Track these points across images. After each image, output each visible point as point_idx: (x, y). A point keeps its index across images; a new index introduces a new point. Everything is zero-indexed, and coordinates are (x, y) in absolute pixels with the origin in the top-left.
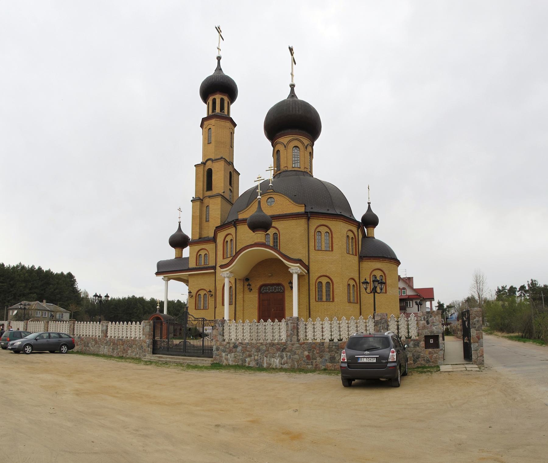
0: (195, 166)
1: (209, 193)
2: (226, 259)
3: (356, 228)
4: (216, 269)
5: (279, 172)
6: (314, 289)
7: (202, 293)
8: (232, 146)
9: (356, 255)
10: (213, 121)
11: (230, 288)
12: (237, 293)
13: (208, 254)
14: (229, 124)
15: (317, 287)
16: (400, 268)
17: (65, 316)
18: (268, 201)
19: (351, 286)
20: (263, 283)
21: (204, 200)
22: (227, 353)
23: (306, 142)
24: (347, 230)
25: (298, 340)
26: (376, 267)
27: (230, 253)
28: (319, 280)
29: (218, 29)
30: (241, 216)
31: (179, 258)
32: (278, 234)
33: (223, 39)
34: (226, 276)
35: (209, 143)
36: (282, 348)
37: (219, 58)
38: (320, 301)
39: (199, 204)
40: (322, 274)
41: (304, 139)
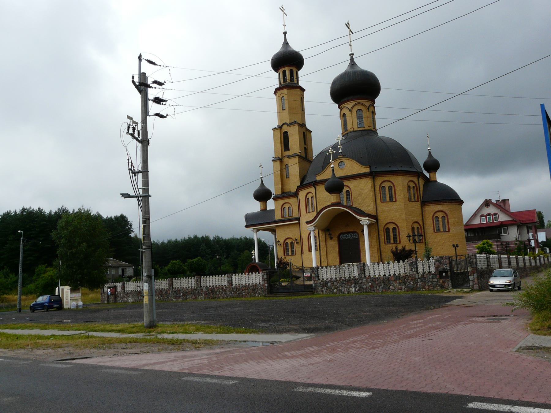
0: (272, 129)
1: (287, 153)
2: (309, 213)
5: (346, 132)
7: (289, 241)
8: (303, 110)
9: (418, 201)
10: (285, 91)
11: (315, 237)
12: (321, 241)
13: (291, 206)
14: (298, 92)
15: (385, 232)
16: (464, 207)
17: (128, 270)
18: (340, 164)
19: (416, 228)
23: (367, 103)
24: (407, 181)
25: (365, 276)
26: (438, 210)
28: (387, 227)
29: (282, 9)
30: (319, 178)
31: (264, 210)
32: (350, 191)
34: (311, 230)
37: (285, 33)
38: (389, 243)
39: (279, 163)
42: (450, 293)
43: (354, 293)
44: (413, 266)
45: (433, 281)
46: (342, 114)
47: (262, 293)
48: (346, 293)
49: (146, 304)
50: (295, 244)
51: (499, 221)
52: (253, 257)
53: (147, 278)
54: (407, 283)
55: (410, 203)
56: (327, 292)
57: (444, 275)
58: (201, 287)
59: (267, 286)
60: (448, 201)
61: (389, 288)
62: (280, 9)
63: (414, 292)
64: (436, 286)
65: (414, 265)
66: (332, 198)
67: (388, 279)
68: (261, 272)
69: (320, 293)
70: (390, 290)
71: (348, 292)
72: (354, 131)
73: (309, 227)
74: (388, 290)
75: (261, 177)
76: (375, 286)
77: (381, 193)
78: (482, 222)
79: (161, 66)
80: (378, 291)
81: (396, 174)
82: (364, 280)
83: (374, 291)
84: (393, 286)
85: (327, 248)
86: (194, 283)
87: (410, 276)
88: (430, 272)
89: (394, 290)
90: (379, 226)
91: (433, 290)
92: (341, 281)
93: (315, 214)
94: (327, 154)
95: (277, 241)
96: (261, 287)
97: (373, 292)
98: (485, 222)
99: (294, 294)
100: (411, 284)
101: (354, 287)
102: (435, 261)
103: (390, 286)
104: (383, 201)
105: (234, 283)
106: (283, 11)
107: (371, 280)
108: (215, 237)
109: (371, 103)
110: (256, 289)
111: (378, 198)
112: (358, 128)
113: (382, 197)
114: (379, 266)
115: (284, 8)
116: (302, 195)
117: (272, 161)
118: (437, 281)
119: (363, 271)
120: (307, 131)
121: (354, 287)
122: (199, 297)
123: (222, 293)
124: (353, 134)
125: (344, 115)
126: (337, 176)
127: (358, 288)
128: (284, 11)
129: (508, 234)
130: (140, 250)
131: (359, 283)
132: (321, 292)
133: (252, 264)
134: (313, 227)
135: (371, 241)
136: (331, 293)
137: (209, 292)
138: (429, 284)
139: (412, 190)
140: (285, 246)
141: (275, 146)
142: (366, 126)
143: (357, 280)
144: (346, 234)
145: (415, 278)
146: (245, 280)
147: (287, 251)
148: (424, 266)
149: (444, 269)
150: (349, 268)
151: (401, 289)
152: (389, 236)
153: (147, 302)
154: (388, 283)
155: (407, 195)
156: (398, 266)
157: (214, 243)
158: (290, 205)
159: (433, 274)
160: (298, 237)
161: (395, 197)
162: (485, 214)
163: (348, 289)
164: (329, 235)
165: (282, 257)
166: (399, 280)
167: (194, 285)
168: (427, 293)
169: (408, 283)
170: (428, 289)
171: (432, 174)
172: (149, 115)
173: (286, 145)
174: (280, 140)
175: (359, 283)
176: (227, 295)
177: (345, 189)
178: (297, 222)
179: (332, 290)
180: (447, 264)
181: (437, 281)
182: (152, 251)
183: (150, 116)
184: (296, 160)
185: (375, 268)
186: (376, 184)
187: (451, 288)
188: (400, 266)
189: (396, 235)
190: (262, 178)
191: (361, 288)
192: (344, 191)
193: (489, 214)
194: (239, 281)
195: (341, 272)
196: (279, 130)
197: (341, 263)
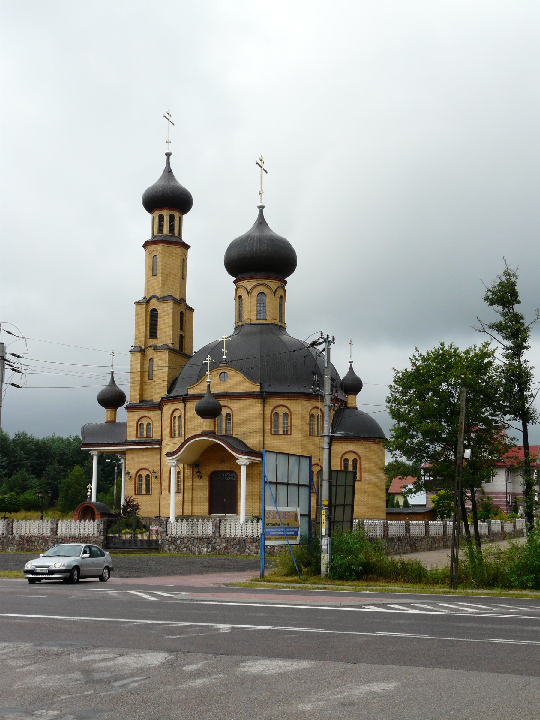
1: (152, 342)
2: (173, 439)
4: (161, 445)
5: (240, 324)
7: (144, 474)
8: (183, 278)
10: (159, 247)
12: (186, 480)
14: (179, 250)
18: (221, 376)
21: (146, 351)
23: (274, 284)
24: (310, 408)
25: (220, 535)
26: (348, 450)
29: (168, 117)
32: (231, 414)
34: (172, 464)
35: (154, 275)
36: (209, 541)
37: (168, 155)
46: (238, 295)
48: (197, 553)
52: (88, 494)
55: (312, 438)
58: (12, 534)
59: (102, 538)
61: (244, 551)
66: (205, 425)
68: (96, 520)
71: (200, 553)
73: (170, 461)
75: (112, 370)
76: (229, 547)
77: (273, 421)
80: (232, 553)
82: (218, 540)
84: (249, 549)
85: (194, 492)
86: (3, 529)
92: (193, 538)
93: (182, 440)
94: (204, 362)
95: (127, 471)
101: (207, 547)
104: (275, 432)
105: (59, 532)
107: (226, 540)
108: (19, 434)
111: (268, 427)
112: (257, 319)
113: (273, 427)
116: (168, 409)
119: (218, 529)
120: (187, 310)
121: (207, 547)
122: (8, 547)
123: (42, 544)
124: (248, 328)
125: (240, 297)
127: (211, 548)
131: (212, 542)
132: (168, 551)
134: (174, 461)
136: (180, 552)
137: (23, 542)
139: (316, 420)
140: (137, 480)
141: (136, 329)
142: (270, 317)
144: (228, 474)
146: (75, 529)
147: (139, 487)
151: (257, 553)
155: (307, 427)
157: (16, 447)
158: (149, 420)
161: (291, 429)
163: (200, 549)
165: (131, 497)
166: (256, 543)
167: (3, 531)
173: (153, 332)
175: (212, 542)
177: (224, 411)
178: (158, 446)
184: (165, 355)
186: (266, 409)
190: (113, 372)
191: (214, 548)
194: (66, 529)
195: (193, 528)
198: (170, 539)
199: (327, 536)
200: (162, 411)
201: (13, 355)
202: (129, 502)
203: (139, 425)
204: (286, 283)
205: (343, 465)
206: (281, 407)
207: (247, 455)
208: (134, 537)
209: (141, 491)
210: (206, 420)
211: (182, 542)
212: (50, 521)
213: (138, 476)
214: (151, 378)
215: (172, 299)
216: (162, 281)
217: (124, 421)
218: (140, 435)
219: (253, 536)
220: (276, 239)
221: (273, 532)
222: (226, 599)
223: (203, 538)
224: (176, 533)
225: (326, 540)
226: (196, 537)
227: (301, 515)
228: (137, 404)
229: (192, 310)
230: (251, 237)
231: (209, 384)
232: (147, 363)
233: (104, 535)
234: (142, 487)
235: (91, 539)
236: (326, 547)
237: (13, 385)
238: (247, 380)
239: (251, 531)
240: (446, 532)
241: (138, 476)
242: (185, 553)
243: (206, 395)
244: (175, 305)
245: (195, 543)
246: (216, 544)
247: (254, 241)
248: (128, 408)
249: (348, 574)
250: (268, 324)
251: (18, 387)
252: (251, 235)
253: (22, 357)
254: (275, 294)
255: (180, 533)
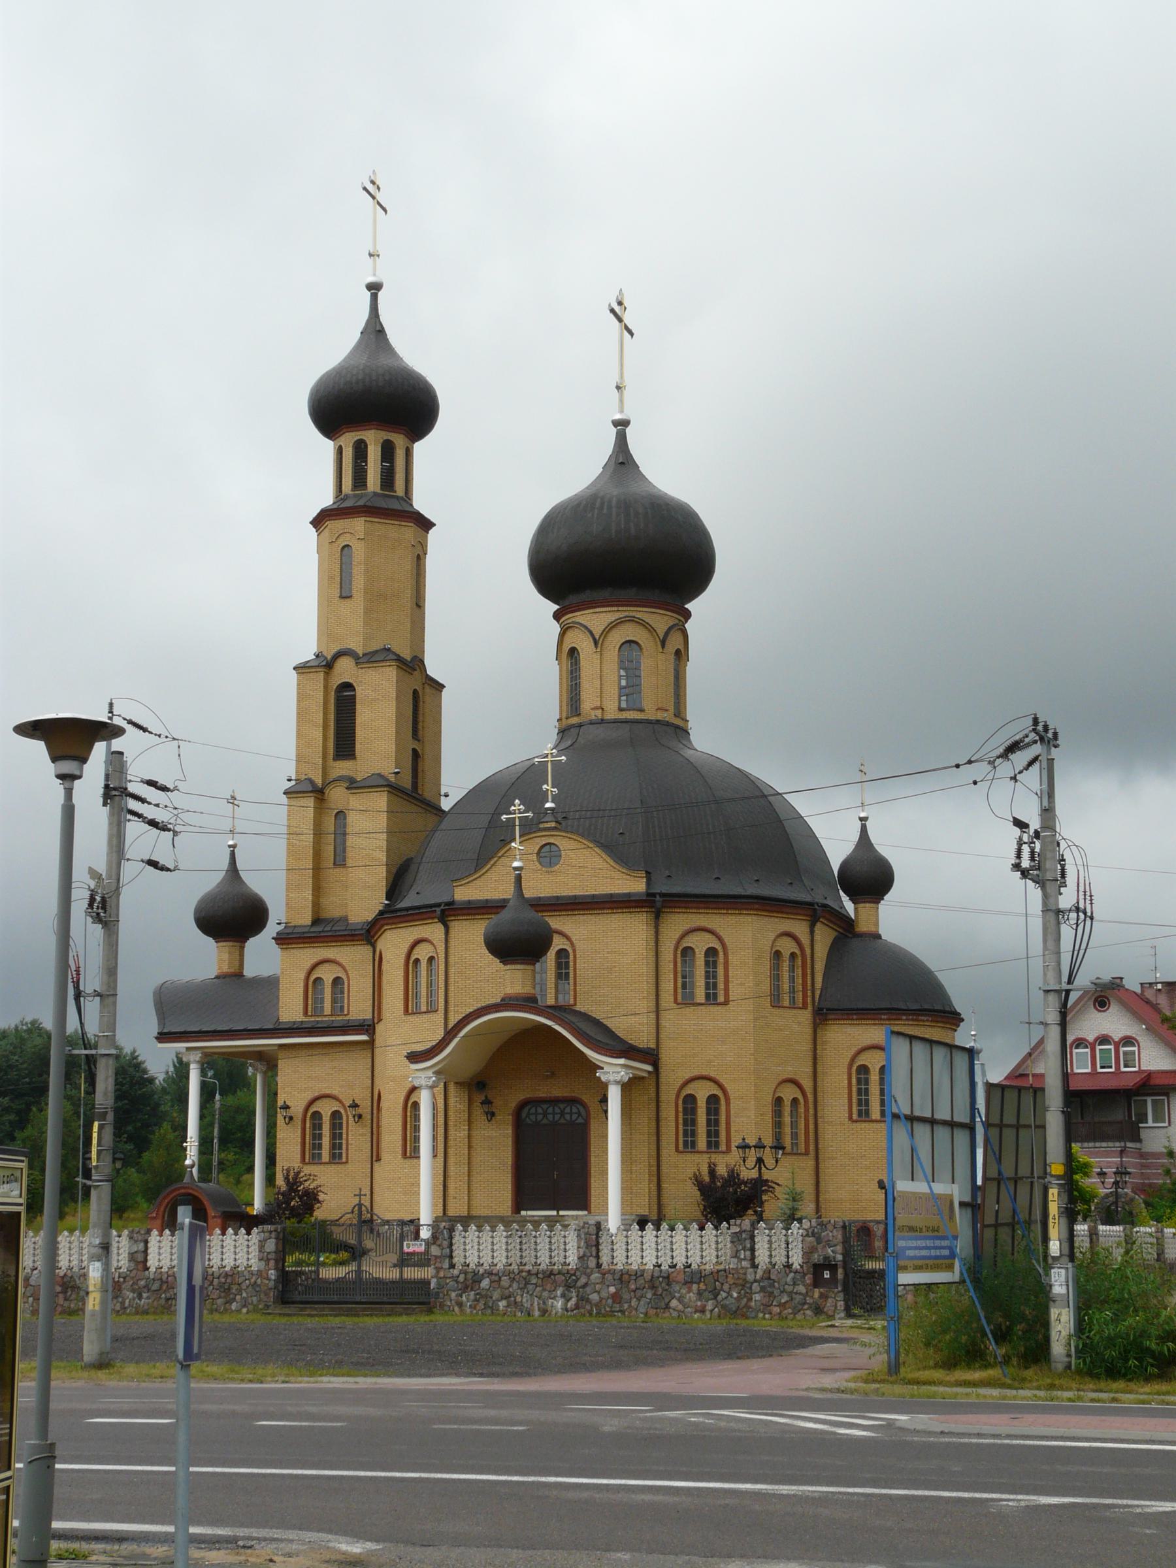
0: (294, 669)
1: (343, 768)
2: (415, 1017)
3: (804, 923)
5: (574, 720)
6: (672, 1118)
7: (326, 1109)
8: (419, 604)
9: (805, 1007)
10: (358, 524)
12: (451, 1123)
14: (408, 531)
15: (681, 1109)
20: (528, 1096)
22: (460, 1292)
23: (660, 620)
24: (772, 936)
25: (599, 1266)
27: (427, 997)
28: (688, 1090)
29: (371, 190)
30: (463, 894)
33: (385, 210)
34: (423, 1083)
35: (345, 596)
36: (567, 1280)
37: (374, 288)
40: (696, 1073)
41: (655, 615)
42: (831, 1329)
43: (559, 1314)
44: (741, 1244)
45: (795, 1291)
46: (566, 647)
47: (255, 1302)
48: (537, 1313)
49: (94, 1311)
50: (348, 1120)
51: (1140, 1072)
53: (100, 1250)
54: (722, 1292)
56: (475, 1308)
57: (827, 1274)
59: (273, 1277)
60: (904, 1014)
61: (667, 1307)
62: (365, 189)
63: (735, 1321)
64: (800, 1307)
65: (745, 1239)
67: (667, 1278)
69: (453, 1310)
70: (671, 1310)
71: (544, 1312)
72: (602, 721)
73: (419, 1074)
74: (664, 1313)
75: (231, 843)
76: (626, 1296)
78: (1077, 1068)
79: (159, 736)
80: (634, 1312)
81: (735, 909)
82: (596, 1276)
83: (622, 1312)
84: (680, 1300)
85: (473, 1154)
87: (731, 1272)
88: (788, 1266)
89: (683, 1312)
90: (663, 1087)
91: (792, 1320)
94: (504, 817)
96: (253, 1280)
97: (620, 1314)
98: (1089, 1070)
99: (364, 1309)
100: (732, 1297)
101: (563, 1296)
102: (805, 1234)
103: (673, 1299)
104: (685, 999)
105: (152, 1262)
106: (374, 197)
107: (617, 1276)
109: (677, 621)
110: (234, 1288)
111: (667, 986)
112: (621, 709)
114: (642, 1237)
115: (377, 183)
117: (284, 793)
118: (804, 1291)
119: (594, 1248)
121: (563, 1296)
125: (573, 651)
126: (526, 896)
128: (379, 197)
129: (1170, 1125)
130: (78, 1182)
131: (579, 1284)
132: (456, 1309)
133: (184, 1188)
134: (430, 1073)
135: (631, 1139)
136: (489, 1311)
138: (783, 1301)
139: (786, 965)
140: (308, 1125)
141: (299, 735)
142: (652, 706)
143: (574, 1275)
144: (545, 1106)
145: (745, 1279)
147: (314, 1144)
148: (774, 1246)
149: (826, 1258)
150: (550, 1237)
152: (694, 1122)
153: (97, 1308)
154: (666, 1290)
156: (699, 1239)
159: (796, 1272)
160: (361, 1095)
162: (1091, 1038)
164: (482, 1103)
168: (770, 1326)
169: (724, 1295)
170: (780, 1314)
171: (866, 908)
172: (127, 857)
174: (321, 715)
175: (579, 1284)
176: (123, 1303)
177: (558, 943)
178: (364, 1038)
179: (494, 1301)
180: (835, 1246)
181: (804, 1291)
182: (113, 1186)
183: (128, 860)
184: (381, 800)
185: (629, 1241)
187: (842, 1315)
188: (704, 1241)
189: (717, 1123)
190: (234, 846)
191: (583, 1299)
192: (551, 955)
193: (1104, 1039)
195: (524, 1247)
196: (322, 674)
197: (518, 1206)
198: (462, 1276)
199: (1065, 1259)
200: (374, 946)
201: (151, 783)
202: (295, 1183)
203: (310, 983)
204: (687, 615)
205: (854, 1081)
206: (698, 933)
207: (626, 1058)
208: (359, 1272)
209: (320, 1155)
210: (513, 967)
211: (495, 1285)
212: (126, 1232)
213: (309, 1114)
214: (340, 861)
215: (395, 658)
216: (367, 611)
217: (265, 972)
218: (315, 1009)
219: (690, 1266)
220: (668, 504)
221: (911, 1248)
222: (1122, 1434)
223: (552, 1273)
224: (476, 1260)
225: (1063, 1271)
226: (534, 1271)
227: (962, 1204)
228: (306, 930)
229: (439, 687)
230: (602, 498)
231: (520, 874)
232: (329, 823)
233: (276, 1269)
234: (320, 1145)
235: (241, 1280)
236: (1063, 1290)
237: (153, 864)
238: (612, 863)
239: (684, 1253)
240: (1163, 1252)
241: (309, 1114)
242: (505, 1314)
243: (511, 903)
244: (402, 673)
245: (530, 1287)
246: (588, 1289)
247: (610, 507)
248: (285, 939)
249: (1132, 1362)
250: (649, 722)
251: (163, 868)
252: (602, 494)
253: (176, 789)
254: (663, 643)
255: (487, 1260)
